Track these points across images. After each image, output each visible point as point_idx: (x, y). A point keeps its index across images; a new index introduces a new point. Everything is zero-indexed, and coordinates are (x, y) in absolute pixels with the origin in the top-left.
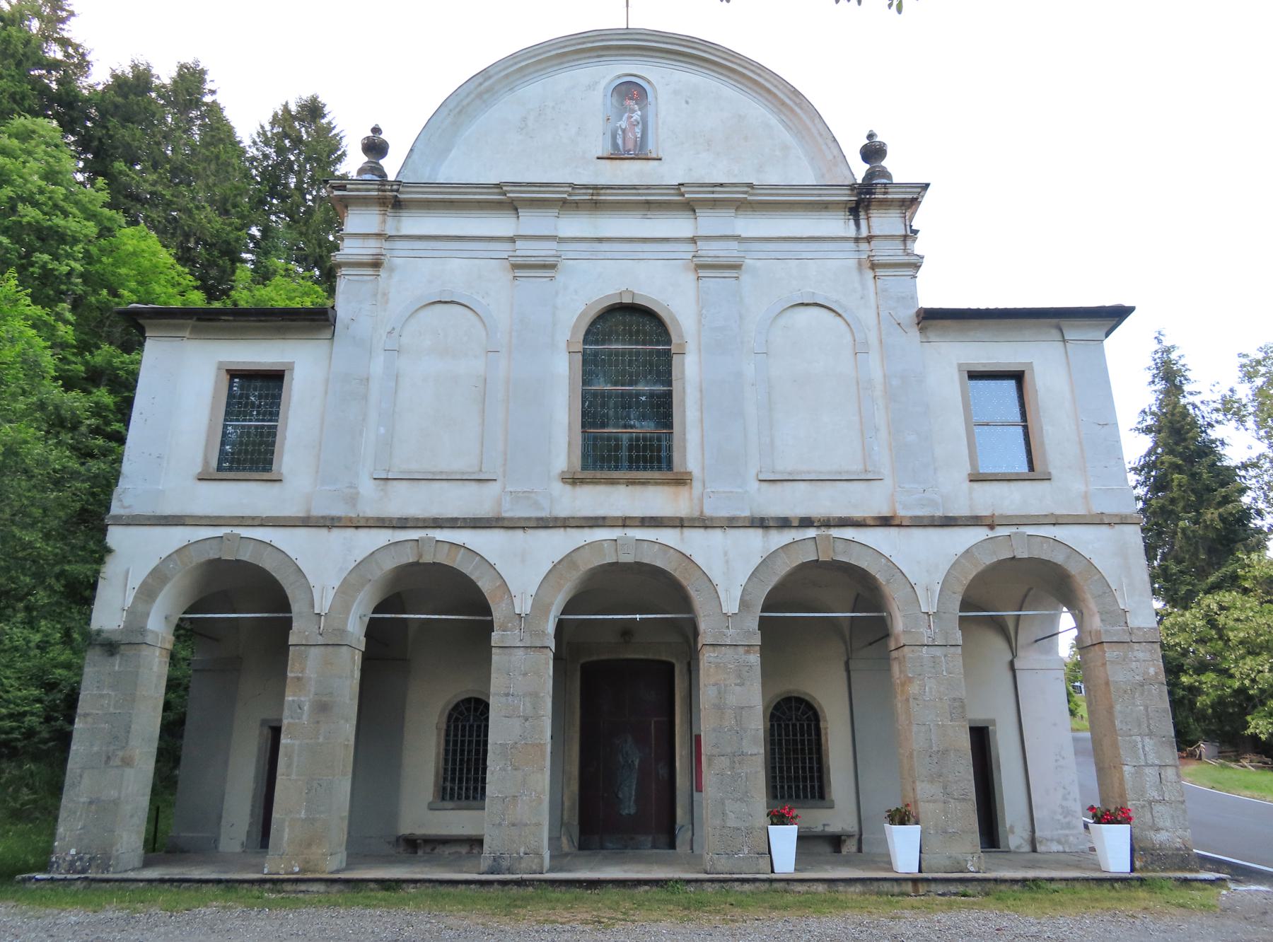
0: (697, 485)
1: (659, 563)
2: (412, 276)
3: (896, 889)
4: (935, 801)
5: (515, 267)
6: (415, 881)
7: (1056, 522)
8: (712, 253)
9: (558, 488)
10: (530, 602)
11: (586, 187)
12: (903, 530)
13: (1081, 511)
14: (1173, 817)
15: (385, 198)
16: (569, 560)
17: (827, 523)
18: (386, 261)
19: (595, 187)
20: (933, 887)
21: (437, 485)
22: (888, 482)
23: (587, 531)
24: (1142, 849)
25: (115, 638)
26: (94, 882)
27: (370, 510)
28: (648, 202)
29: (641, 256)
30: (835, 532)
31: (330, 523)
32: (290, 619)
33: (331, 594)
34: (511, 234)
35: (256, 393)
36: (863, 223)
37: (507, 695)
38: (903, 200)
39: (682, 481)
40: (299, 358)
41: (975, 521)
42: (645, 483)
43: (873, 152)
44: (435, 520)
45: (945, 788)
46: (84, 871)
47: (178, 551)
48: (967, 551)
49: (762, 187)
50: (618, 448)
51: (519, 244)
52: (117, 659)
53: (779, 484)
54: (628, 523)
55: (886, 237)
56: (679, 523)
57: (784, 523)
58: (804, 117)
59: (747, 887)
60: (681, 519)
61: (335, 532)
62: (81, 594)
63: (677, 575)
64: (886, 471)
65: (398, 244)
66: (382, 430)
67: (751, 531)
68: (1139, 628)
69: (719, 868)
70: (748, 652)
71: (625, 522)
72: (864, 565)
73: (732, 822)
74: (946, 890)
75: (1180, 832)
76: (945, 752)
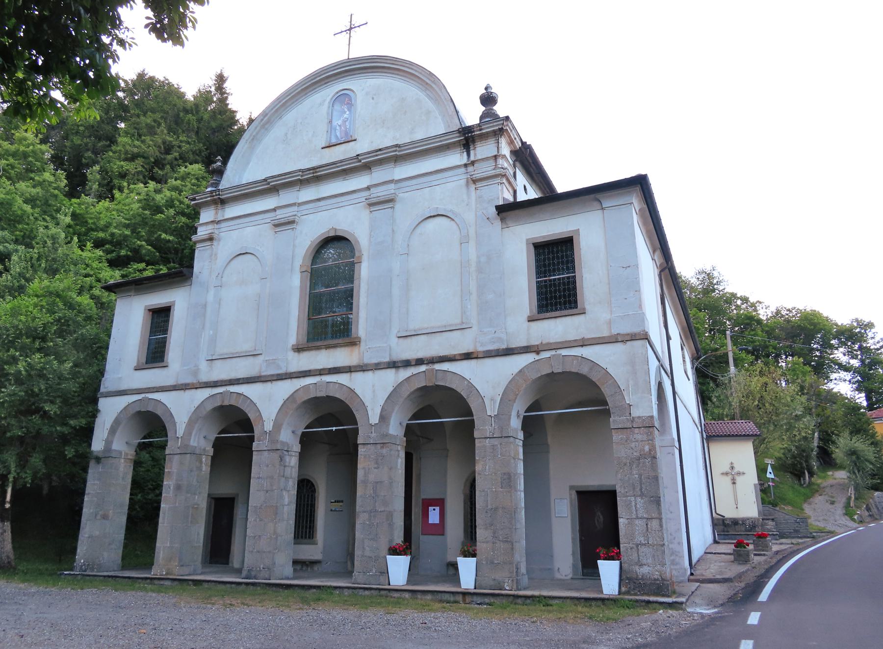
0: (362, 344)
1: (337, 396)
2: (230, 240)
3: (452, 599)
4: (487, 542)
5: (276, 226)
6: (208, 581)
7: (583, 343)
8: (375, 195)
9: (292, 355)
10: (272, 423)
11: (309, 169)
12: (480, 361)
13: (606, 333)
14: (654, 556)
15: (215, 200)
16: (292, 398)
17: (432, 361)
18: (215, 236)
19: (314, 168)
20: (475, 598)
21: (234, 360)
22: (475, 328)
23: (302, 379)
24: (628, 578)
25: (100, 455)
26: (90, 578)
27: (204, 378)
28: (344, 170)
29: (341, 204)
30: (437, 367)
31: (184, 387)
32: (357, 429)
33: (184, 425)
34: (273, 207)
35: (160, 317)
36: (472, 152)
37: (259, 478)
38: (494, 131)
39: (354, 343)
40: (177, 298)
41: (526, 350)
42: (335, 346)
43: (488, 99)
44: (230, 380)
45: (494, 533)
46: (85, 571)
47: (125, 408)
48: (520, 371)
49: (405, 145)
50: (326, 326)
51: (278, 212)
52: (100, 466)
53: (413, 338)
54: (397, 365)
55: (483, 160)
56: (349, 370)
57: (407, 364)
58: (437, 90)
59: (367, 593)
60: (350, 367)
61: (187, 391)
62: (88, 432)
63: (347, 402)
64: (474, 322)
65: (223, 225)
66: (211, 332)
67: (389, 371)
68: (639, 417)
69: (359, 581)
70: (382, 447)
71: (321, 372)
72: (454, 387)
73: (368, 553)
74: (482, 601)
75: (659, 567)
76: (496, 509)
